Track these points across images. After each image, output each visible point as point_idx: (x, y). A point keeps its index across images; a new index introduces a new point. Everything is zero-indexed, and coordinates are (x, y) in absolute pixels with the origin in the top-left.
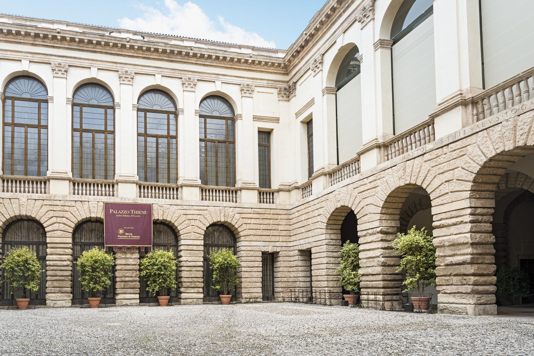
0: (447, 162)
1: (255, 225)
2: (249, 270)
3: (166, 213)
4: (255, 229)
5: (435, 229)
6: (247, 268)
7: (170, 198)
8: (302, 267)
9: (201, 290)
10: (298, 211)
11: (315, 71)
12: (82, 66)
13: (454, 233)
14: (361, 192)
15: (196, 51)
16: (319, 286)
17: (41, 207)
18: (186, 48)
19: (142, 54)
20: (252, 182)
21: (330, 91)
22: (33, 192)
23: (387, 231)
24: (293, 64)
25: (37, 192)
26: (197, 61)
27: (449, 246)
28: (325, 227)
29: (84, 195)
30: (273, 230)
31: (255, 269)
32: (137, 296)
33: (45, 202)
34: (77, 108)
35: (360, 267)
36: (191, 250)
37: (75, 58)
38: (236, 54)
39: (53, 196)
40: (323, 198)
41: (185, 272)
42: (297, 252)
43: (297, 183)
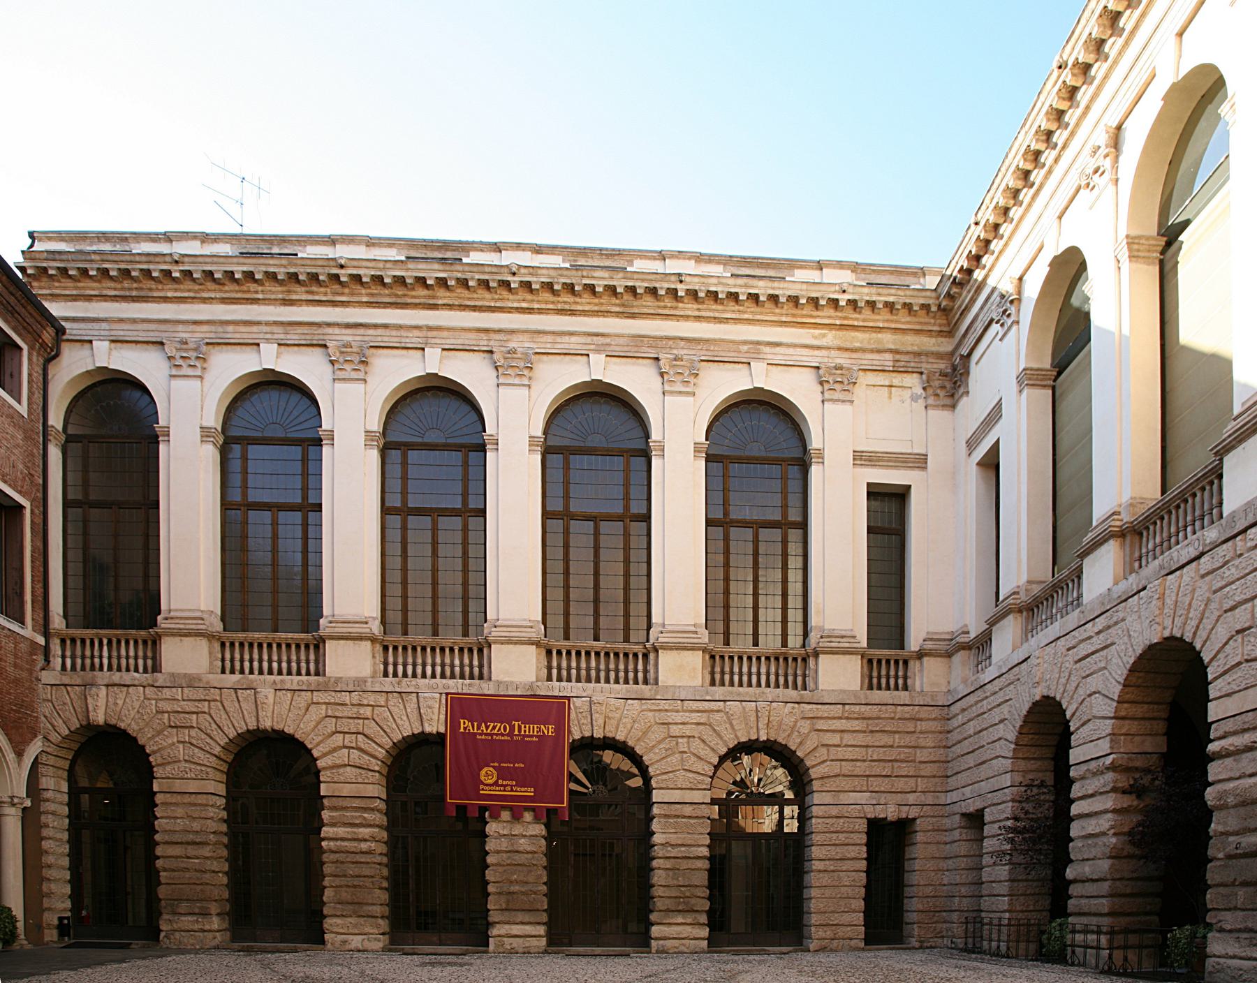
0: (1242, 577)
1: (850, 749)
2: (832, 868)
3: (614, 722)
4: (852, 760)
5: (1212, 760)
6: (827, 862)
7: (626, 682)
8: (969, 860)
9: (704, 919)
10: (964, 710)
11: (1002, 325)
12: (403, 345)
13: (1247, 773)
14: (1080, 660)
15: (693, 284)
16: (994, 909)
17: (307, 709)
18: (668, 278)
19: (553, 303)
20: (849, 633)
21: (1037, 380)
22: (289, 673)
23: (1130, 765)
24: (960, 306)
25: (299, 673)
26: (699, 310)
27: (1235, 806)
28: (1010, 754)
29: (390, 678)
30: (902, 761)
31: (848, 865)
32: (541, 930)
33: (318, 697)
34: (395, 455)
35: (1072, 861)
36: (677, 816)
37: (386, 326)
38: (804, 287)
39: (332, 680)
40: (1011, 676)
41: (660, 872)
42: (957, 817)
43: (968, 633)
